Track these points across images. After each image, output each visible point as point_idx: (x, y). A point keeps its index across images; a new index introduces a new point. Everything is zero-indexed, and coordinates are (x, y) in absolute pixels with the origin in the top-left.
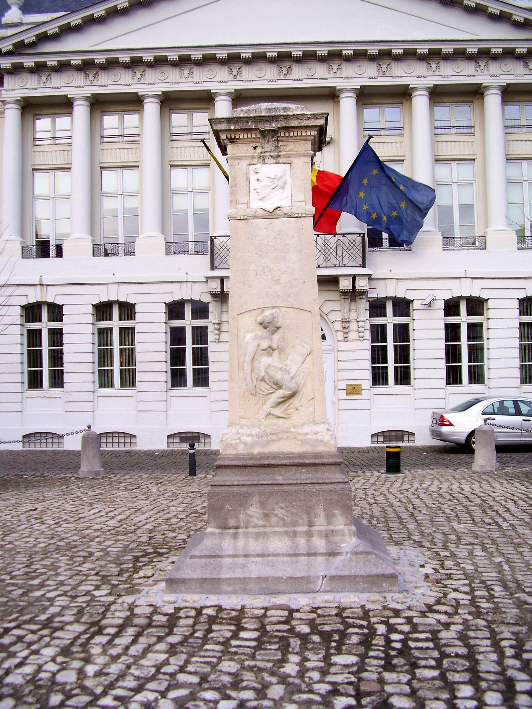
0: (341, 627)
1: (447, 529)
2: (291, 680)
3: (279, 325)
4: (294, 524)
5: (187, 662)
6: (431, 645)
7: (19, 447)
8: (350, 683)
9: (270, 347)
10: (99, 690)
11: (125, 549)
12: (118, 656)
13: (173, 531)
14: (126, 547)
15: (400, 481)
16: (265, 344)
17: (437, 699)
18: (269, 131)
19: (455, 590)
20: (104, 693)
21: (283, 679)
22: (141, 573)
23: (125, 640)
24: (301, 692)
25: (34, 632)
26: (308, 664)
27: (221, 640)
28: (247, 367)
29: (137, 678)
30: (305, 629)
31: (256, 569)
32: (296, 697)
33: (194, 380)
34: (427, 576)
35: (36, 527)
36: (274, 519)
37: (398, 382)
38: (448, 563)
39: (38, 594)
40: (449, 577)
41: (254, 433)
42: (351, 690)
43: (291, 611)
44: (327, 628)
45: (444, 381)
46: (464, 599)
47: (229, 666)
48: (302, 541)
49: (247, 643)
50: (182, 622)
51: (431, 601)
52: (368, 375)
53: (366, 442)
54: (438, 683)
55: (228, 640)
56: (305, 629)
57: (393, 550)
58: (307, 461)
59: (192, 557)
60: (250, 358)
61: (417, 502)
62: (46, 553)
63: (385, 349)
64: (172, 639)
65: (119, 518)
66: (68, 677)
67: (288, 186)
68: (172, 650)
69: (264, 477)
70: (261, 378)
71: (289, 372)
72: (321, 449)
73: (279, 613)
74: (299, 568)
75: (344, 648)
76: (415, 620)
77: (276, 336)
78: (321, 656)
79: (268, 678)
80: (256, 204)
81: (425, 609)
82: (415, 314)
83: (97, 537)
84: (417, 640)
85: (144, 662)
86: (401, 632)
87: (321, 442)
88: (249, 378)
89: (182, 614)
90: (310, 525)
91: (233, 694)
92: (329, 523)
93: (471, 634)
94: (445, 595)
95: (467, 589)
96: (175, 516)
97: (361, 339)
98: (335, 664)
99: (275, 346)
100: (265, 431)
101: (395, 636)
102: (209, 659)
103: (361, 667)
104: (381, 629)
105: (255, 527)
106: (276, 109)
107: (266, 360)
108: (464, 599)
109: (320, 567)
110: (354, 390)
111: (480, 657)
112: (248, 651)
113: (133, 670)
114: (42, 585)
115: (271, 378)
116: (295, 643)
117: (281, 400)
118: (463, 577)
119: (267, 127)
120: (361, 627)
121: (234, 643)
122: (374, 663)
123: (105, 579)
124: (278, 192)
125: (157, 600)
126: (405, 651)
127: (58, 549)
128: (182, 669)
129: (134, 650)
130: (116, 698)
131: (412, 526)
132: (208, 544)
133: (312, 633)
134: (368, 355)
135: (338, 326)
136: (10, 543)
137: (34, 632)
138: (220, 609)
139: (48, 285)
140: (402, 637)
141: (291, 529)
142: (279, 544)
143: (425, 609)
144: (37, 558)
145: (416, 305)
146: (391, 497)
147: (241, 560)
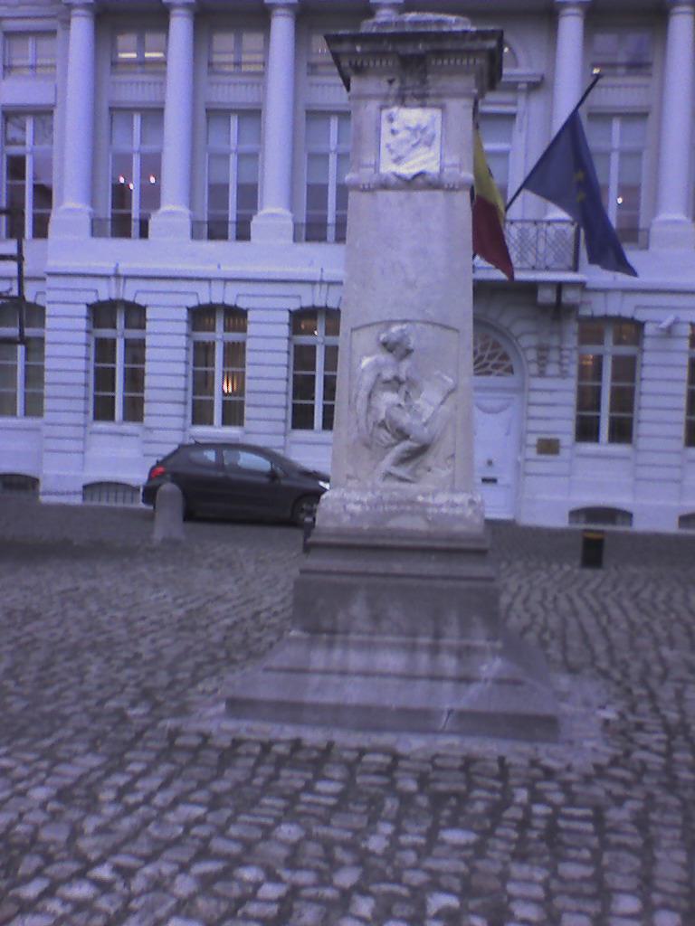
0: (463, 787)
1: (651, 655)
2: (373, 861)
3: (411, 346)
4: (414, 634)
5: (231, 821)
6: (589, 827)
7: (77, 500)
8: (457, 875)
9: (396, 379)
10: (93, 856)
11: (187, 653)
12: (137, 805)
13: (261, 629)
14: (188, 648)
15: (599, 580)
16: (388, 374)
17: (580, 912)
18: (412, 56)
19: (645, 748)
20: (101, 861)
21: (363, 858)
22: (200, 687)
23: (147, 785)
24: (385, 880)
25: (26, 764)
26: (404, 839)
27: (288, 792)
28: (361, 405)
29: (156, 841)
30: (411, 786)
31: (354, 693)
32: (374, 888)
33: (124, 413)
34: (607, 722)
35: (71, 613)
36: (385, 625)
37: (27, 413)
38: (644, 707)
39: (48, 708)
40: (640, 727)
41: (365, 499)
42: (456, 884)
43: (396, 757)
44: (442, 787)
45: (683, 442)
46: (655, 761)
47: (289, 832)
48: (423, 660)
49: (323, 800)
50: (240, 762)
51: (604, 760)
52: (570, 426)
53: (560, 521)
54: (588, 889)
55: (298, 792)
56: (411, 786)
57: (564, 682)
58: (438, 544)
59: (267, 670)
60: (366, 393)
61: (615, 612)
62: (75, 651)
63: (597, 392)
64: (218, 786)
65: (190, 606)
66: (55, 835)
67: (437, 143)
68: (214, 804)
69: (377, 566)
70: (379, 421)
71: (419, 416)
72: (459, 528)
73: (379, 758)
74: (416, 696)
75: (462, 819)
76: (575, 788)
77: (406, 364)
78: (423, 829)
79: (339, 853)
80: (388, 168)
81: (591, 770)
82: (647, 344)
83: (152, 631)
84: (571, 818)
85: (171, 817)
86: (550, 804)
87: (460, 519)
88: (362, 423)
89: (242, 750)
90: (438, 635)
91: (286, 875)
92: (463, 635)
93: (654, 816)
94: (628, 754)
95: (662, 748)
96: (268, 609)
97: (563, 375)
98: (443, 843)
99: (403, 376)
100: (381, 498)
101: (539, 809)
102: (263, 820)
103: (479, 849)
104: (522, 795)
105: (359, 632)
106: (426, 23)
107: (388, 398)
108: (655, 761)
109: (447, 699)
110: (549, 447)
111: (659, 855)
112: (320, 811)
113: (151, 828)
114: (57, 696)
115: (393, 423)
116: (391, 804)
117: (406, 455)
118: (659, 729)
119: (409, 49)
120: (492, 790)
121: (306, 798)
122: (498, 848)
123: (146, 694)
124: (422, 150)
125: (211, 727)
126: (552, 834)
127: (93, 647)
128: (222, 831)
129: (159, 800)
130: (118, 869)
131: (600, 648)
132: (287, 655)
133: (421, 791)
134: (572, 398)
135: (532, 355)
136: (29, 634)
137: (26, 764)
138: (297, 745)
139: (126, 277)
140: (548, 810)
141: (409, 640)
142: (392, 661)
143: (591, 770)
144: (60, 658)
145: (649, 329)
146: (579, 604)
147: (335, 679)
